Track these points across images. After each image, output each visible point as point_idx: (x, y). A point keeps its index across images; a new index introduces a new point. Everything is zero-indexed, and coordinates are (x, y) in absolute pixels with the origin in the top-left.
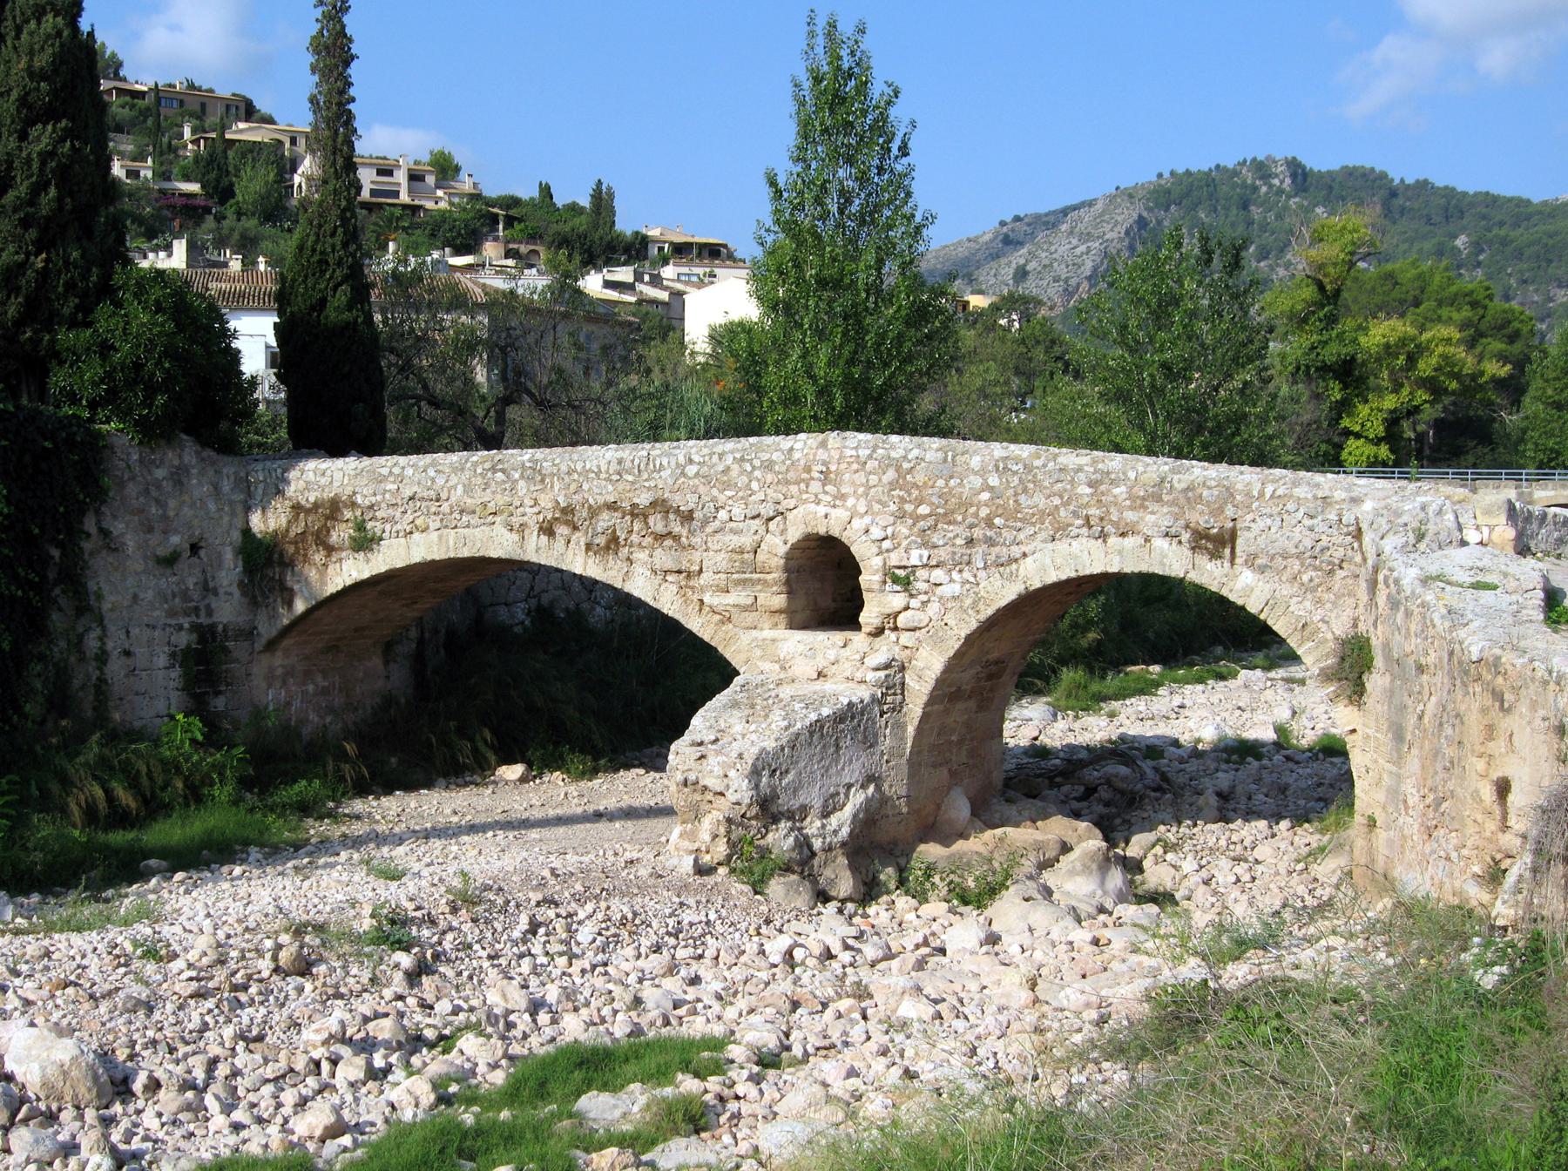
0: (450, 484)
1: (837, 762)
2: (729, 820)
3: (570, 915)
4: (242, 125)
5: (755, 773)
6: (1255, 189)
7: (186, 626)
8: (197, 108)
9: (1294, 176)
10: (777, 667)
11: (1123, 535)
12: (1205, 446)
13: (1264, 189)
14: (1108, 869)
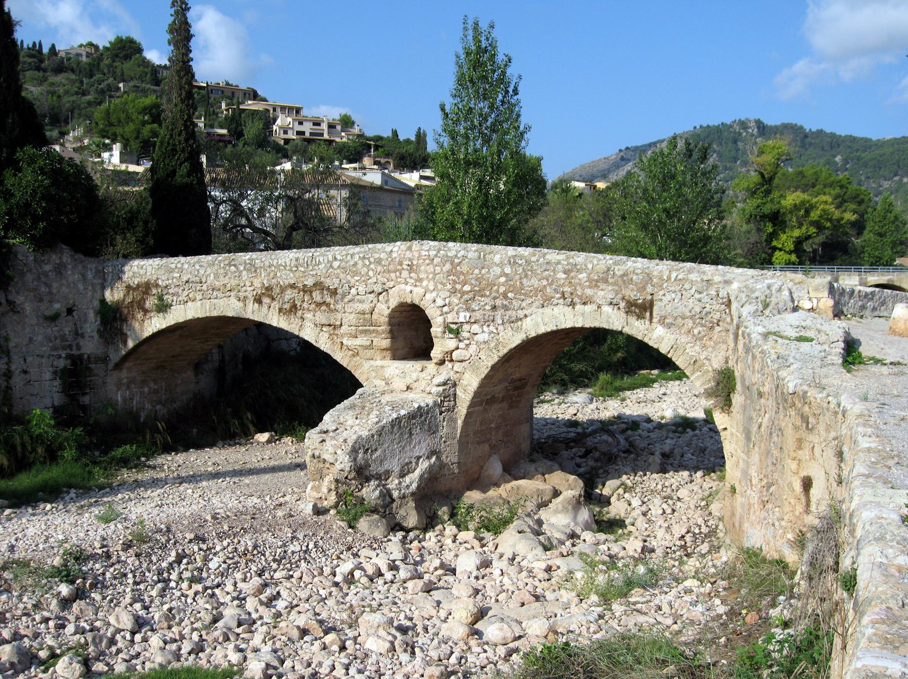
0: (208, 273)
1: (410, 443)
2: (337, 481)
3: (209, 549)
4: (250, 102)
5: (354, 451)
6: (740, 134)
7: (63, 355)
8: (230, 94)
9: (759, 128)
10: (383, 383)
11: (584, 304)
12: (687, 253)
13: (744, 134)
14: (579, 509)
